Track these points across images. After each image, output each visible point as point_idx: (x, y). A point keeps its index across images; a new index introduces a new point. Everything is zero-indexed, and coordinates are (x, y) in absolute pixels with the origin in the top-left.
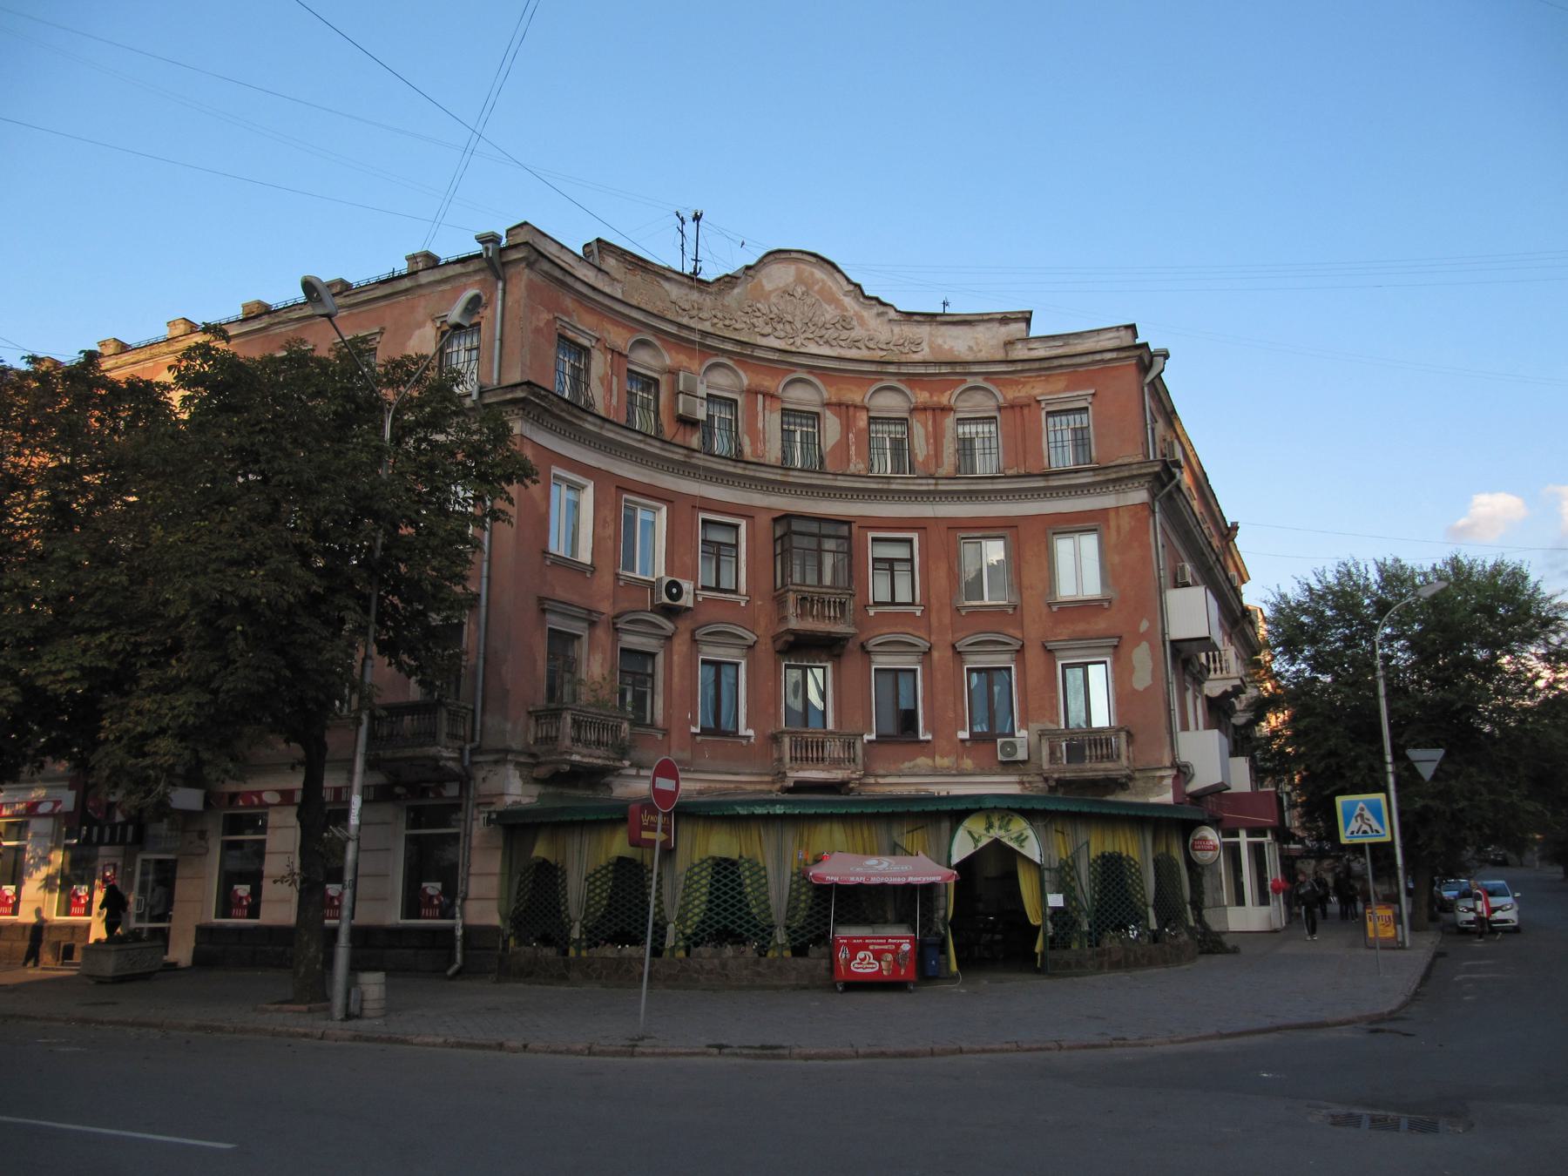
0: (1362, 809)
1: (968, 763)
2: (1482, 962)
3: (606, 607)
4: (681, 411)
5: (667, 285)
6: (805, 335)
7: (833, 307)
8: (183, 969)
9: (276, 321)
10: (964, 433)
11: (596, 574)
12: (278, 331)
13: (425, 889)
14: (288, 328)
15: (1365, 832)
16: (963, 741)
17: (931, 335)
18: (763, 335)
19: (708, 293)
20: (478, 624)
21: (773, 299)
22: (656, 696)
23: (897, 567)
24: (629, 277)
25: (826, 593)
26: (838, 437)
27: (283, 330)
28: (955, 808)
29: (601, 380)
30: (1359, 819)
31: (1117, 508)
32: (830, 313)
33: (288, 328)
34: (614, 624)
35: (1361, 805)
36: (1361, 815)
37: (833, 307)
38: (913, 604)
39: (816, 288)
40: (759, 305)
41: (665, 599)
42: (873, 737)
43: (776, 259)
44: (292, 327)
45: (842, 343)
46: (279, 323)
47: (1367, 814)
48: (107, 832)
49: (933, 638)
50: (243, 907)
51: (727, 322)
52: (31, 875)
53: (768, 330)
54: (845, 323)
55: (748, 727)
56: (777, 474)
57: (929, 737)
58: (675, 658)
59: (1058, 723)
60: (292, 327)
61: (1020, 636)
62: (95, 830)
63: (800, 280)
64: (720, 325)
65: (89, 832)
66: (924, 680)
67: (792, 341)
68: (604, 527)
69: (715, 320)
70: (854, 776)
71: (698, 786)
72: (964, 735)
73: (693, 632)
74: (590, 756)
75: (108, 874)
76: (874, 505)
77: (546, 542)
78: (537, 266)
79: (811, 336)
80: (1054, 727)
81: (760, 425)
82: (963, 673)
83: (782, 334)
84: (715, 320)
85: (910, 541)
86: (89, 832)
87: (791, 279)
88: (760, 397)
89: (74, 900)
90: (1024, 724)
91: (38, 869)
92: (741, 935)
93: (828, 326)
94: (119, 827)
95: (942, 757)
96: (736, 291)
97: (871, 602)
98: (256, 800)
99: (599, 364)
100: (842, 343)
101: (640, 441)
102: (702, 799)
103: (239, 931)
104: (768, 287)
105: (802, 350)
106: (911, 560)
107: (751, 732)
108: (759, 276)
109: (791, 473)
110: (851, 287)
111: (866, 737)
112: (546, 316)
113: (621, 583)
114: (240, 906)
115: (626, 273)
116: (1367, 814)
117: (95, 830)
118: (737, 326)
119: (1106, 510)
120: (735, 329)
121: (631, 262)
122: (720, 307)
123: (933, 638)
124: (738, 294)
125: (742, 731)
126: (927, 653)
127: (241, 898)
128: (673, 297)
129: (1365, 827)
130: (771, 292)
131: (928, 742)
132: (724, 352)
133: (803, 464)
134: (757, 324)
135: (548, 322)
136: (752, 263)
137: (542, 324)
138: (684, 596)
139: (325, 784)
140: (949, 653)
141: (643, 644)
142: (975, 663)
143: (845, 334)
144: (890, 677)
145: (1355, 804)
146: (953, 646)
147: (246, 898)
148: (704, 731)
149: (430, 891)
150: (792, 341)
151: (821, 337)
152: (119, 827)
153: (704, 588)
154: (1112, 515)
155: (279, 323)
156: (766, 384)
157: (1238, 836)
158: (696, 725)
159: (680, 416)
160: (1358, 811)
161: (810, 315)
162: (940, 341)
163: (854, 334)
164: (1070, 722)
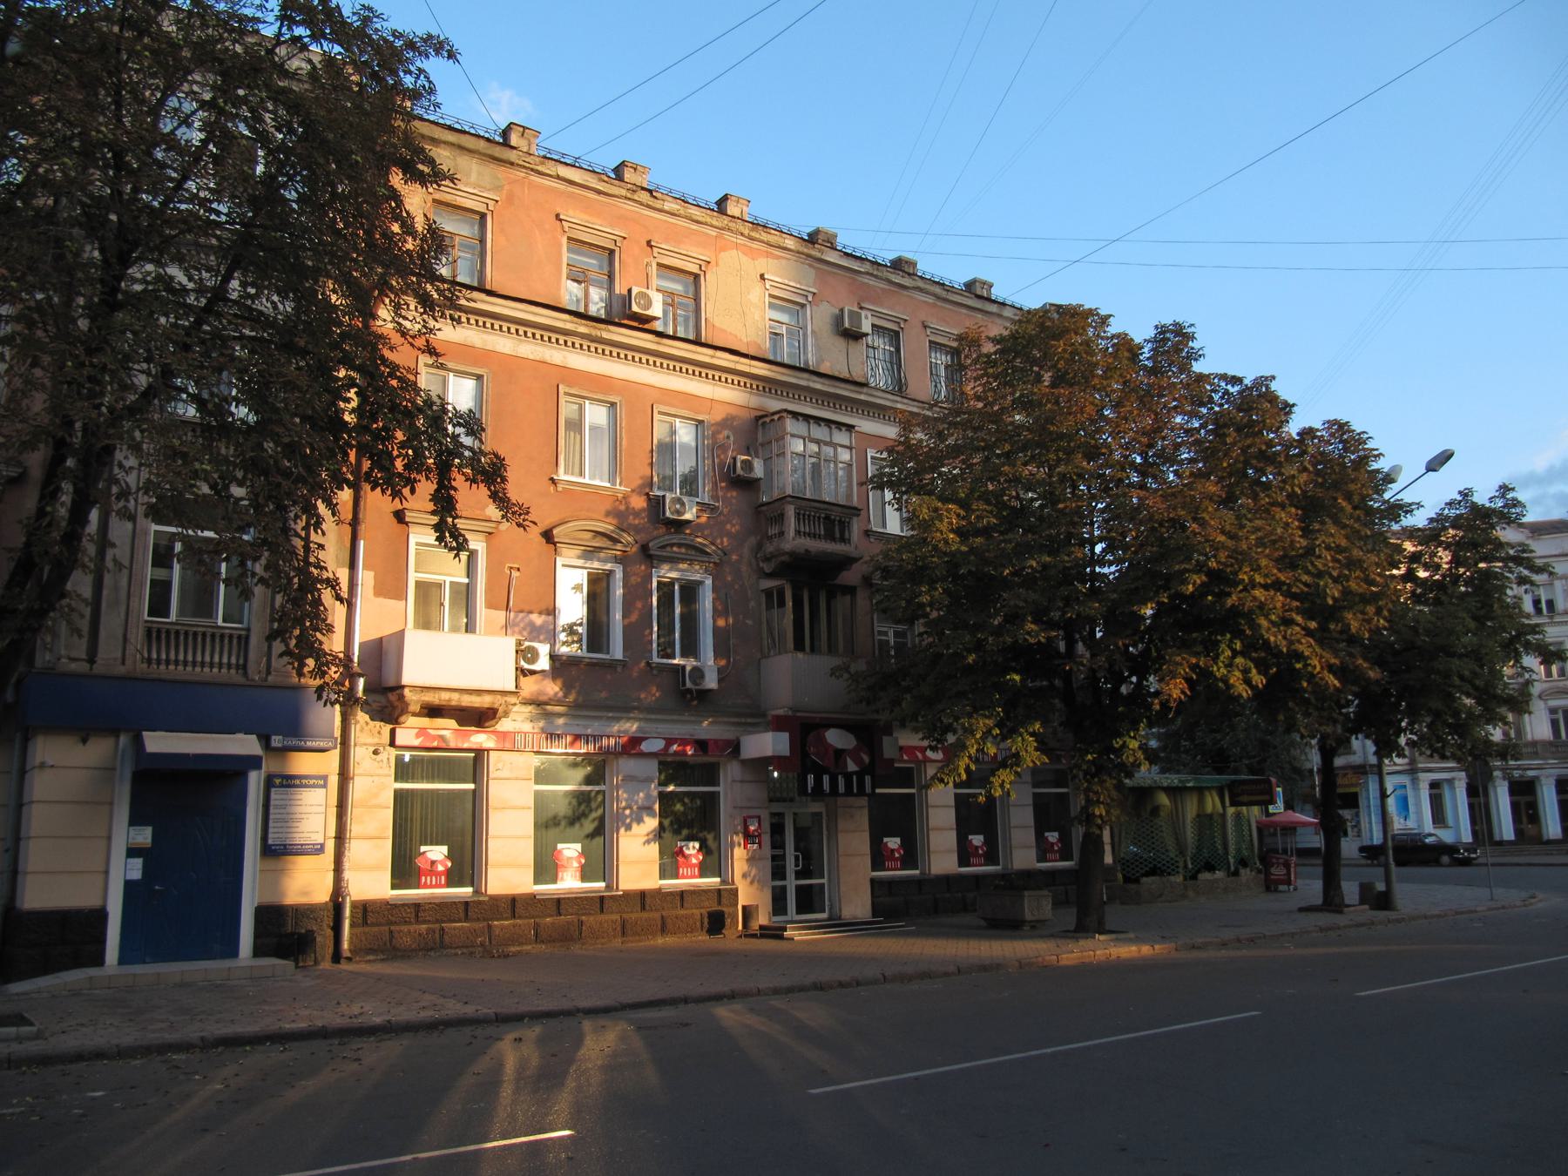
2: (1321, 950)
4: (847, 325)
8: (1549, 842)
9: (875, 273)
12: (866, 281)
13: (1047, 838)
14: (877, 284)
20: (587, 540)
22: (132, 599)
27: (871, 282)
33: (877, 284)
44: (882, 286)
46: (876, 276)
48: (841, 780)
50: (896, 859)
52: (629, 828)
56: (802, 379)
60: (882, 286)
62: (826, 779)
65: (818, 781)
75: (752, 828)
76: (599, 361)
86: (818, 781)
89: (680, 859)
91: (640, 820)
94: (855, 778)
98: (919, 755)
103: (977, 879)
109: (865, 390)
114: (977, 855)
117: (826, 779)
127: (893, 851)
133: (675, 331)
147: (898, 850)
149: (1051, 839)
152: (855, 778)
155: (876, 276)
159: (846, 329)
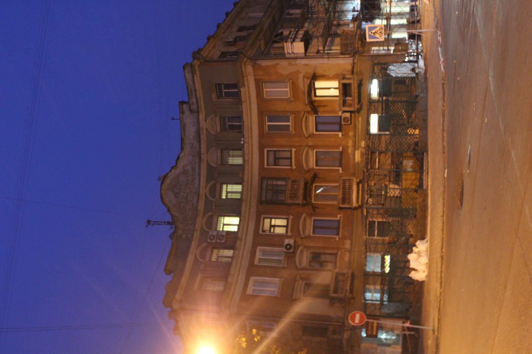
0: (372, 33)
1: (351, 134)
15: (380, 32)
16: (342, 135)
23: (277, 156)
30: (375, 34)
31: (255, 76)
35: (370, 33)
36: (374, 33)
38: (291, 151)
42: (341, 169)
47: (373, 31)
49: (304, 144)
53: (191, 204)
55: (336, 217)
57: (341, 148)
59: (336, 100)
61: (303, 113)
66: (324, 217)
72: (340, 134)
73: (302, 238)
80: (338, 102)
82: (318, 134)
90: (336, 112)
95: (348, 143)
97: (290, 167)
106: (275, 151)
107: (339, 216)
110: (173, 170)
111: (341, 171)
116: (373, 31)
119: (256, 80)
123: (304, 144)
125: (338, 218)
126: (310, 147)
129: (379, 32)
131: (343, 148)
136: (166, 209)
139: (339, 48)
140: (309, 139)
145: (369, 35)
146: (307, 138)
154: (257, 77)
158: (335, 238)
160: (373, 34)
162: (191, 137)
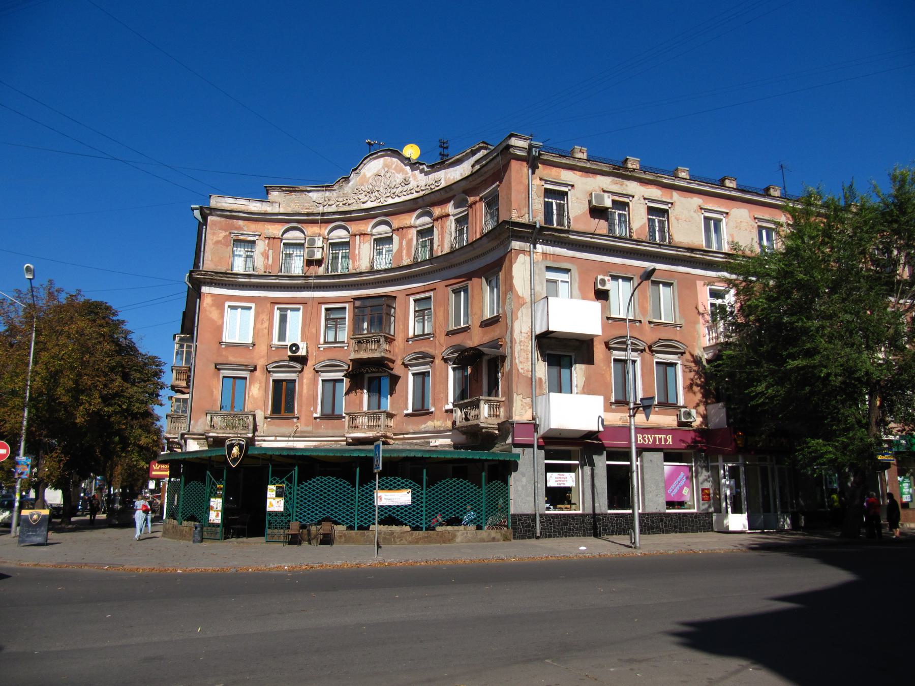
3: (261, 363)
5: (311, 194)
6: (386, 195)
7: (401, 174)
10: (300, 251)
11: (256, 346)
17: (446, 173)
18: (364, 203)
19: (333, 190)
21: (370, 181)
24: (288, 197)
25: (369, 337)
26: (397, 248)
28: (360, 455)
29: (262, 254)
32: (399, 178)
34: (267, 369)
37: (401, 174)
39: (393, 166)
40: (362, 187)
41: (290, 353)
43: (370, 159)
45: (405, 193)
51: (344, 202)
53: (366, 199)
54: (406, 182)
58: (305, 381)
63: (386, 165)
64: (341, 204)
67: (379, 200)
68: (262, 324)
69: (338, 203)
70: (378, 435)
71: (314, 444)
74: (223, 433)
77: (221, 338)
78: (213, 214)
79: (389, 194)
81: (357, 252)
83: (373, 199)
84: (338, 203)
85: (345, 308)
87: (381, 166)
88: (358, 237)
92: (402, 521)
93: (397, 186)
96: (351, 183)
99: (261, 246)
100: (405, 193)
101: (275, 279)
102: (315, 454)
104: (368, 175)
105: (385, 203)
108: (363, 171)
112: (223, 234)
113: (274, 349)
115: (285, 196)
118: (350, 202)
120: (349, 205)
121: (286, 191)
122: (342, 195)
124: (352, 185)
128: (314, 199)
130: (370, 177)
132: (338, 220)
134: (360, 198)
135: (225, 237)
137: (220, 239)
138: (301, 350)
141: (286, 376)
142: (325, 377)
143: (406, 188)
144: (331, 385)
146: (314, 369)
148: (324, 417)
150: (379, 200)
151: (394, 193)
153: (326, 343)
156: (362, 228)
157: (718, 462)
158: (316, 413)
161: (388, 183)
162: (449, 175)
163: (410, 186)
164: (377, 400)
